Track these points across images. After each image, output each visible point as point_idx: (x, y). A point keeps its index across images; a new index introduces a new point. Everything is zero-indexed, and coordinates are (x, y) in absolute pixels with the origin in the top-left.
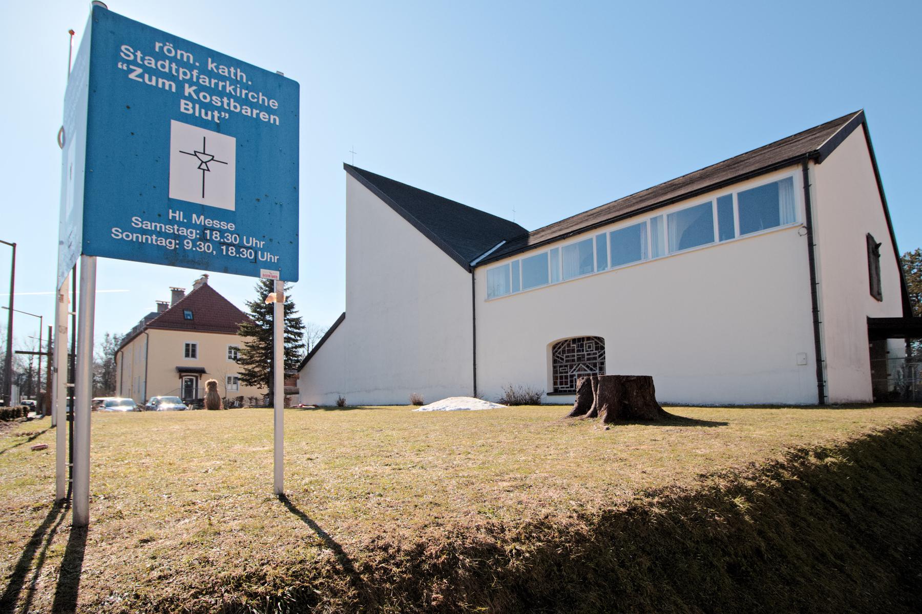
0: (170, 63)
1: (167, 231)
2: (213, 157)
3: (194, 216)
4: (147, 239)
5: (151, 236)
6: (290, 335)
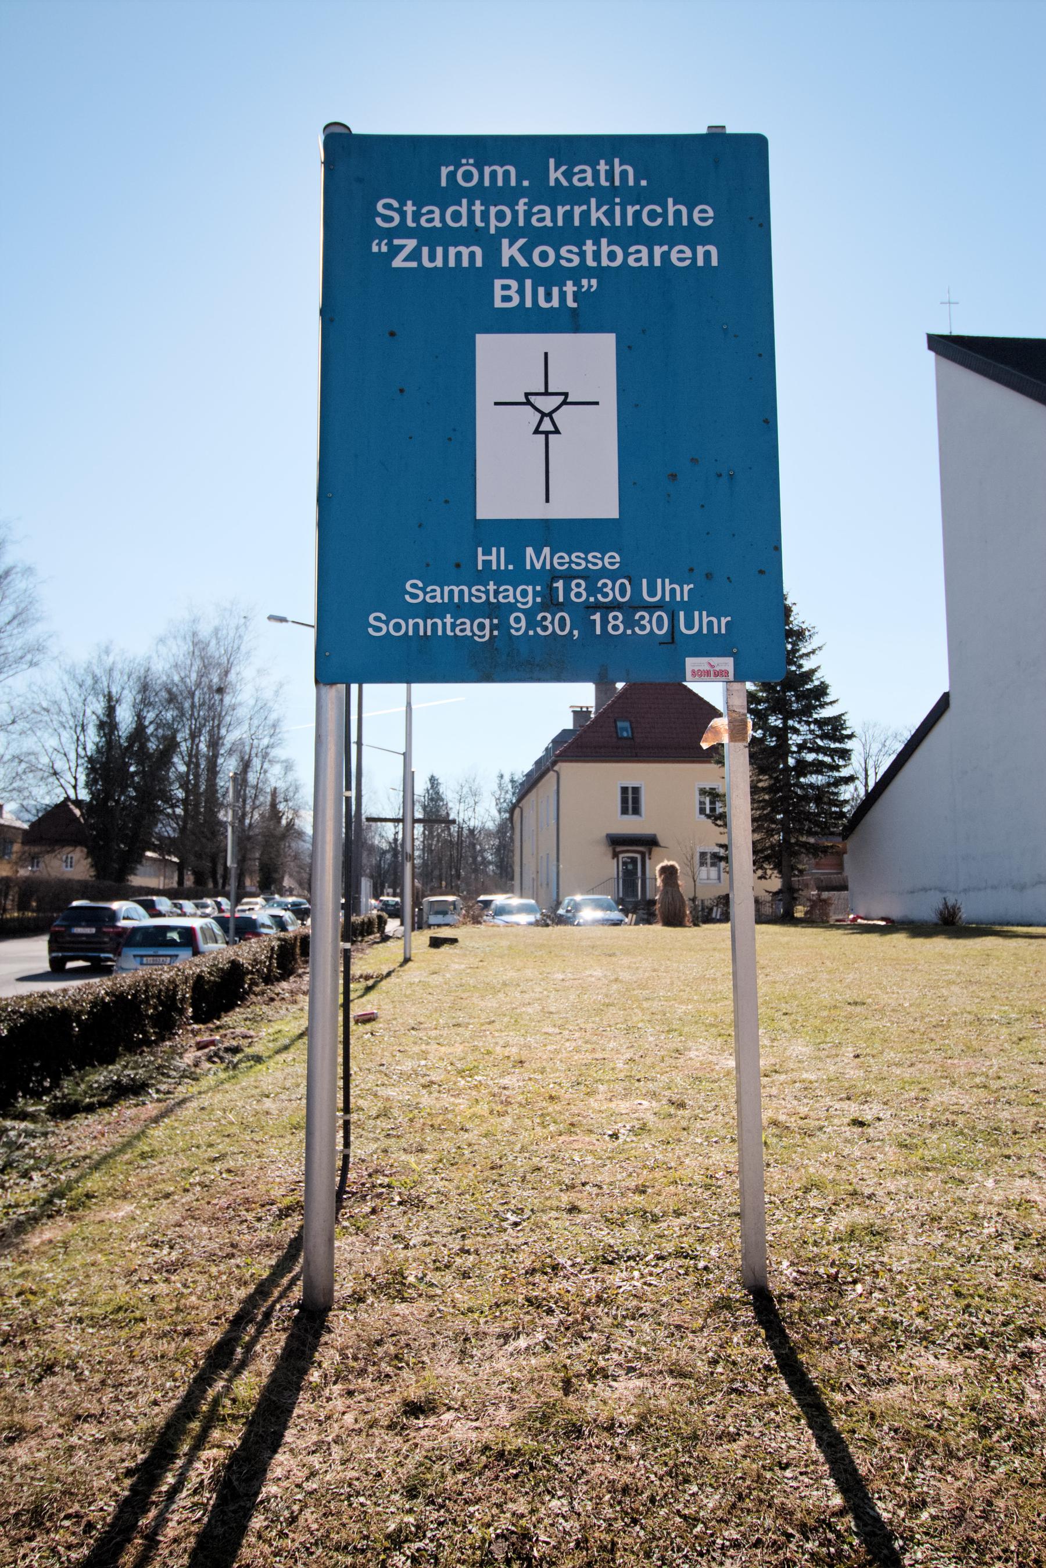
0: (471, 204)
1: (474, 599)
2: (566, 395)
3: (530, 551)
4: (434, 626)
5: (442, 617)
6: (821, 757)
